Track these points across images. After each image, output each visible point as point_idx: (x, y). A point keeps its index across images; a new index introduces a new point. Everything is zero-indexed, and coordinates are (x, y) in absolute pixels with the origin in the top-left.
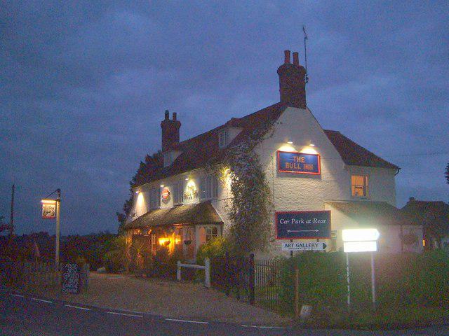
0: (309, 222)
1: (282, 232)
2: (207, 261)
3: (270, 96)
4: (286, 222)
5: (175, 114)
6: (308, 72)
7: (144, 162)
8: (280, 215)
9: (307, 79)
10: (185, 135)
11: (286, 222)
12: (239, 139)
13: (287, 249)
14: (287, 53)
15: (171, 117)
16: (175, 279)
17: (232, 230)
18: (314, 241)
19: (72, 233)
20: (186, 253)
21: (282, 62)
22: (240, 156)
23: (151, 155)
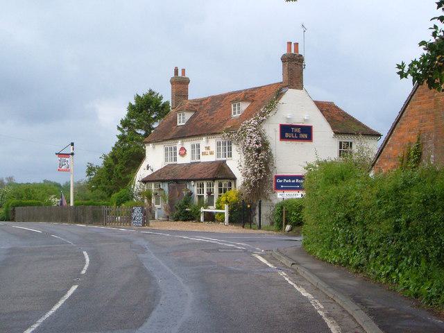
0: (293, 181)
1: (193, 146)
2: (226, 206)
3: (276, 74)
4: (281, 181)
5: (183, 71)
6: (306, 62)
7: (134, 103)
8: (277, 177)
9: (305, 65)
10: (195, 93)
11: (281, 181)
12: (247, 115)
13: (281, 197)
14: (290, 43)
15: (180, 74)
16: (199, 221)
17: (244, 184)
18: (296, 192)
19: (58, 182)
20: (429, 53)
21: (285, 52)
22: (251, 130)
23: (141, 96)
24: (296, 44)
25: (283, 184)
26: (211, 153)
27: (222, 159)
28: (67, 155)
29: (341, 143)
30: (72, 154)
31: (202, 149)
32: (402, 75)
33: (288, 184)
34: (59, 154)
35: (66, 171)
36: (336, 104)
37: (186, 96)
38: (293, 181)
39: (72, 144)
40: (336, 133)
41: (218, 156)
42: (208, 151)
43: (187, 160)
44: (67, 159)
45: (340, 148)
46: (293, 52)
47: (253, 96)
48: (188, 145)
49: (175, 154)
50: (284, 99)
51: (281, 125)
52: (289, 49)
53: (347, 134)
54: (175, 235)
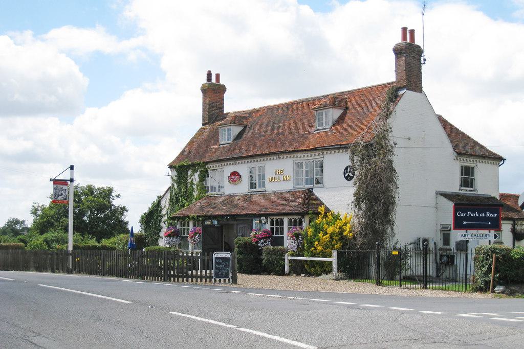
0: (482, 215)
4: (463, 215)
5: (218, 76)
6: (427, 54)
11: (463, 215)
15: (214, 80)
18: (486, 232)
24: (412, 32)
25: (466, 218)
28: (64, 182)
29: (462, 167)
38: (482, 215)
39: (72, 168)
40: (460, 154)
42: (281, 177)
43: (243, 188)
45: (462, 174)
46: (408, 41)
47: (345, 101)
48: (243, 168)
50: (401, 104)
52: (404, 38)
53: (470, 155)
54: (356, 305)
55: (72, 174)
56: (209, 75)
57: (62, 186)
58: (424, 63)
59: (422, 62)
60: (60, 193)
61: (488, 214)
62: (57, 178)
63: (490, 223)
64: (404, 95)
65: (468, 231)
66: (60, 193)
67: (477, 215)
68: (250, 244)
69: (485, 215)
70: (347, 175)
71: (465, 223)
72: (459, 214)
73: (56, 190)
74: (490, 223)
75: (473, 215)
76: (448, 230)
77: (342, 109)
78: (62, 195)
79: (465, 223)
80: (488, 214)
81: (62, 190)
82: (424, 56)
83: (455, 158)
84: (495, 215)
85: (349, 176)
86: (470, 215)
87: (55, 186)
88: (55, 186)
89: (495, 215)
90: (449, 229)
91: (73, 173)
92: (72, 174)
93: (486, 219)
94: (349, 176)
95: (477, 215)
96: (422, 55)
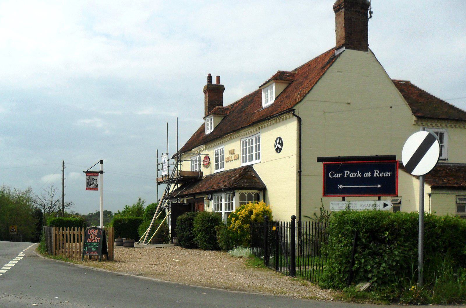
0: (368, 175)
4: (338, 176)
5: (218, 78)
9: (371, 13)
11: (338, 176)
15: (214, 82)
25: (342, 180)
26: (236, 158)
27: (248, 163)
28: (96, 173)
30: (102, 172)
31: (226, 155)
32: (333, 208)
33: (356, 180)
34: (87, 172)
35: (94, 189)
36: (413, 82)
37: (221, 103)
38: (368, 175)
39: (102, 162)
41: (245, 160)
44: (96, 178)
49: (200, 165)
51: (317, 162)
55: (102, 167)
56: (210, 77)
57: (93, 177)
58: (371, 17)
59: (369, 15)
60: (92, 183)
61: (376, 173)
62: (88, 171)
63: (379, 186)
64: (342, 55)
65: (346, 198)
66: (92, 183)
67: (359, 175)
68: (190, 218)
69: (373, 174)
70: (276, 147)
71: (341, 187)
72: (332, 175)
73: (88, 180)
74: (379, 186)
75: (352, 175)
76: (398, 204)
77: (286, 83)
78: (93, 184)
79: (341, 187)
80: (376, 173)
81: (93, 180)
82: (370, 9)
83: (415, 123)
84: (388, 174)
85: (278, 148)
86: (348, 176)
87: (88, 177)
88: (88, 177)
89: (388, 174)
90: (398, 202)
91: (103, 166)
92: (102, 167)
93: (373, 180)
94: (278, 148)
95: (359, 175)
96: (369, 8)
